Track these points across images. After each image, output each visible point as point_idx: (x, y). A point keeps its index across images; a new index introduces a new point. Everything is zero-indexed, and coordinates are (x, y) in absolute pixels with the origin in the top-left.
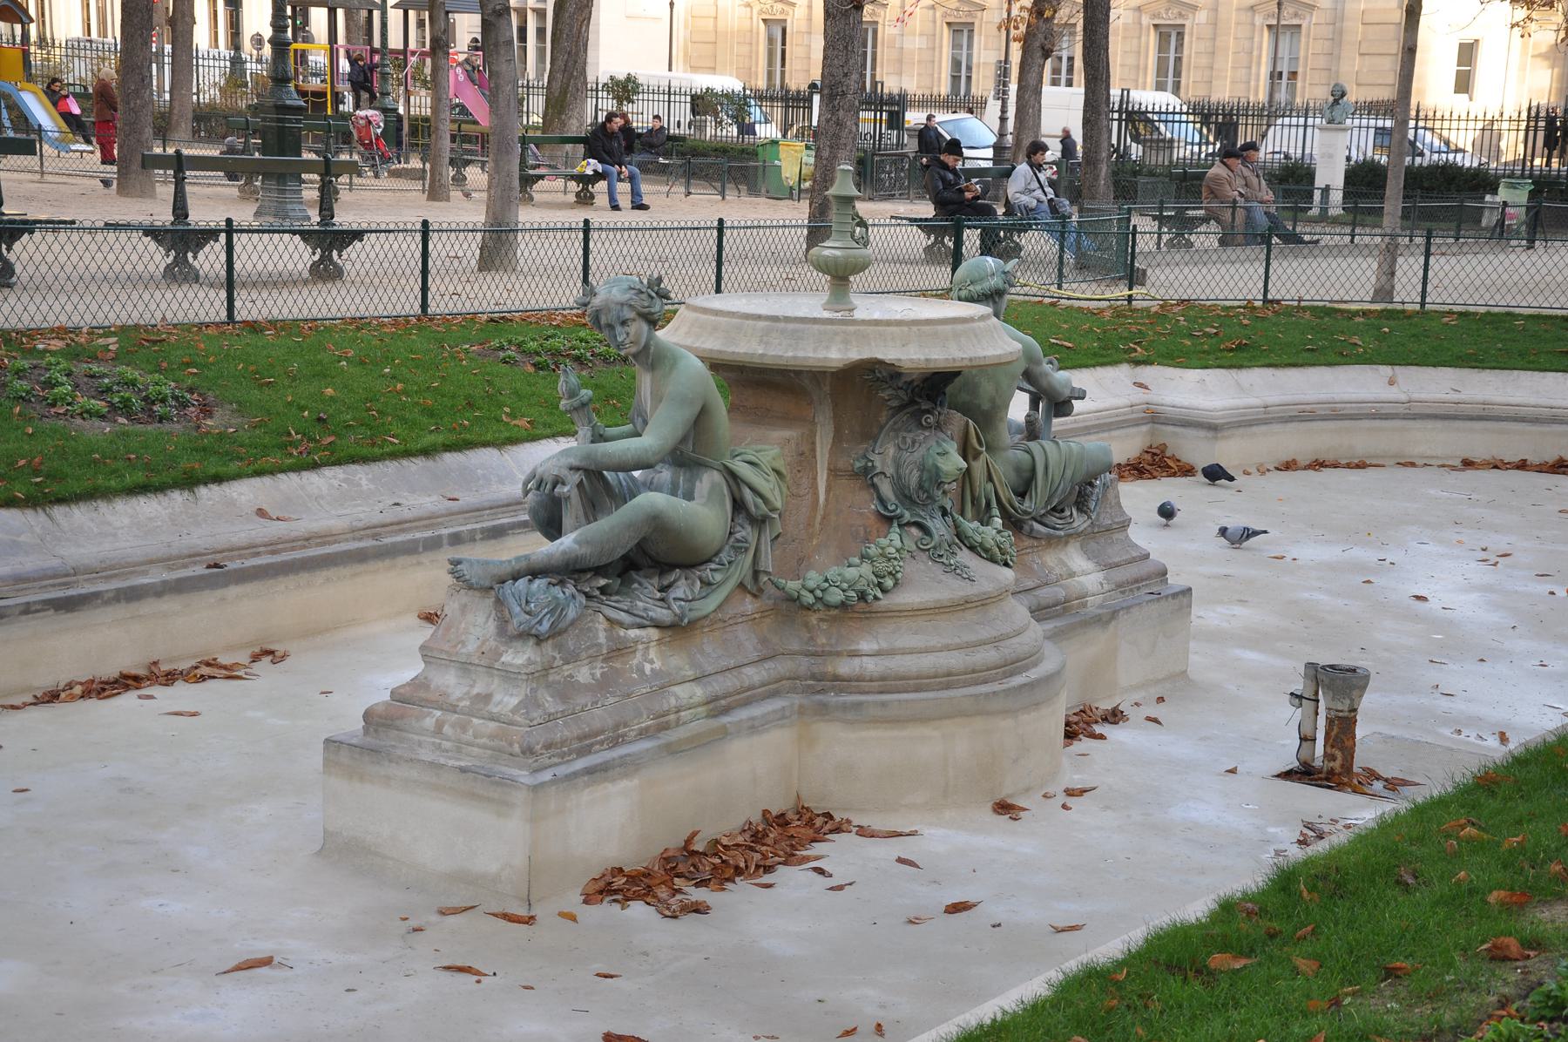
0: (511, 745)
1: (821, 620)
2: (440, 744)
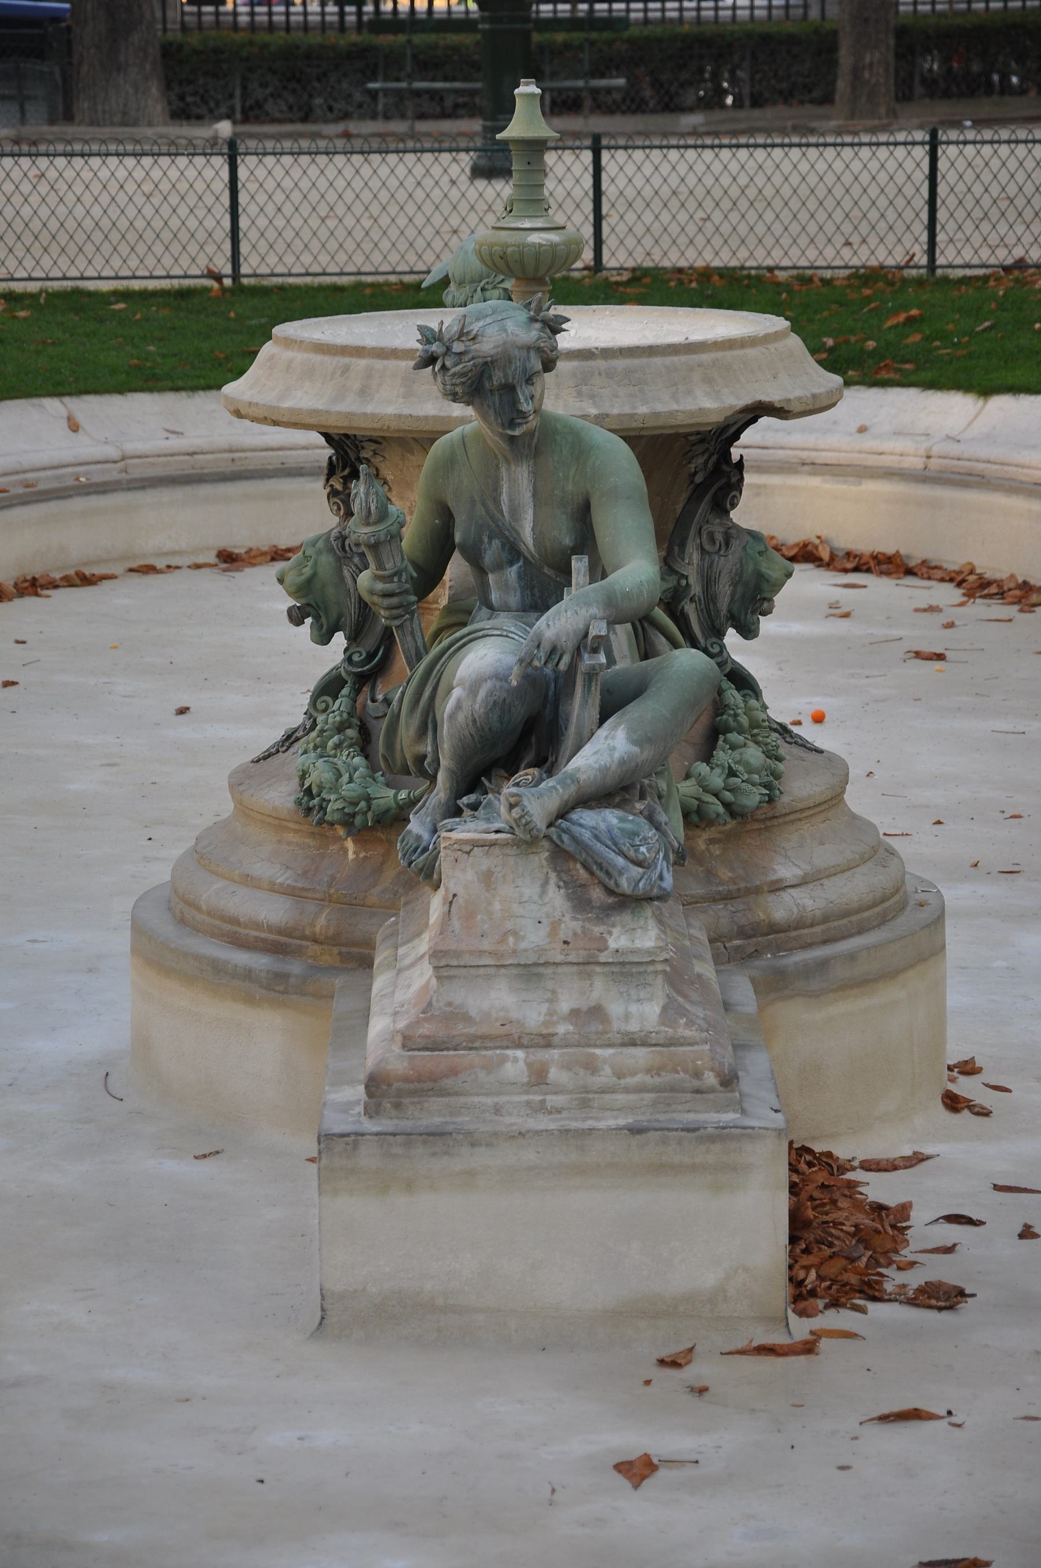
0: (697, 1075)
1: (712, 841)
2: (543, 1101)
